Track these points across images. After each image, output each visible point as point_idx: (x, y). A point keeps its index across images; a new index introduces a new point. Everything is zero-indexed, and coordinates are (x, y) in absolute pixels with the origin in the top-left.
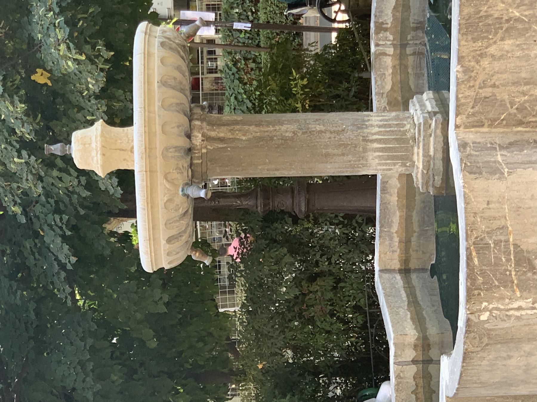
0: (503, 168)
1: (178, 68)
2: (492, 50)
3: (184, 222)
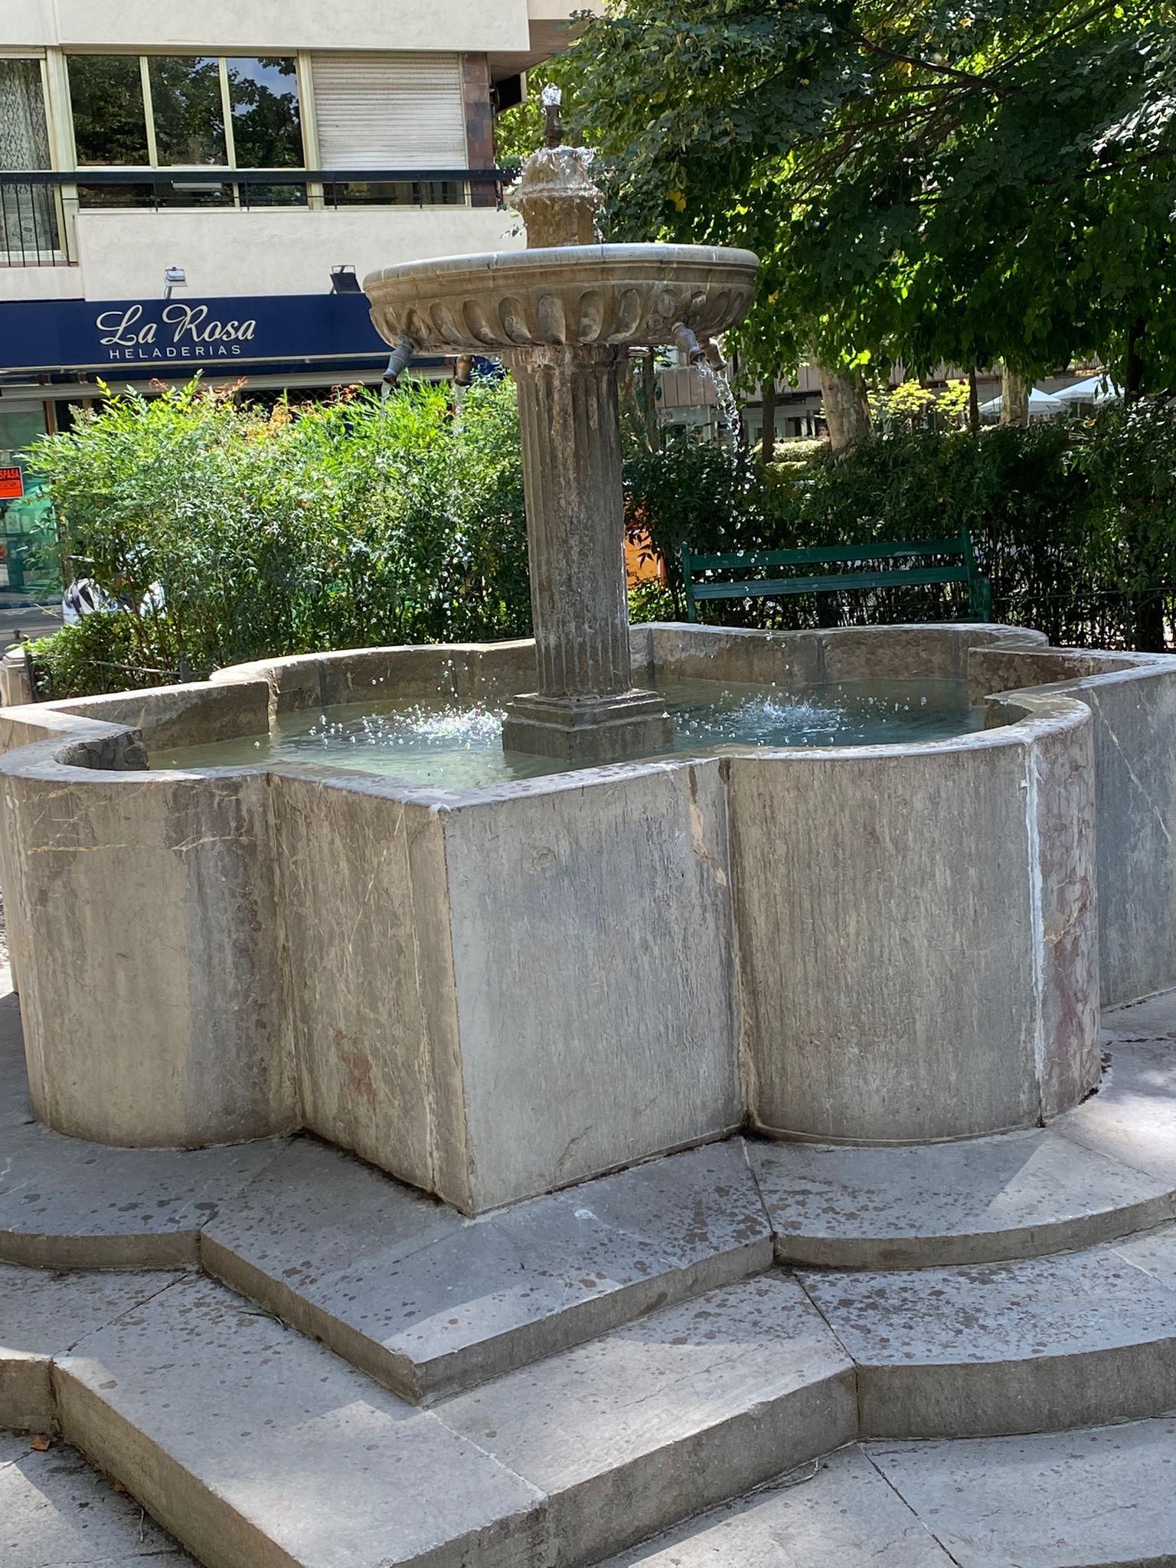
0: (187, 843)
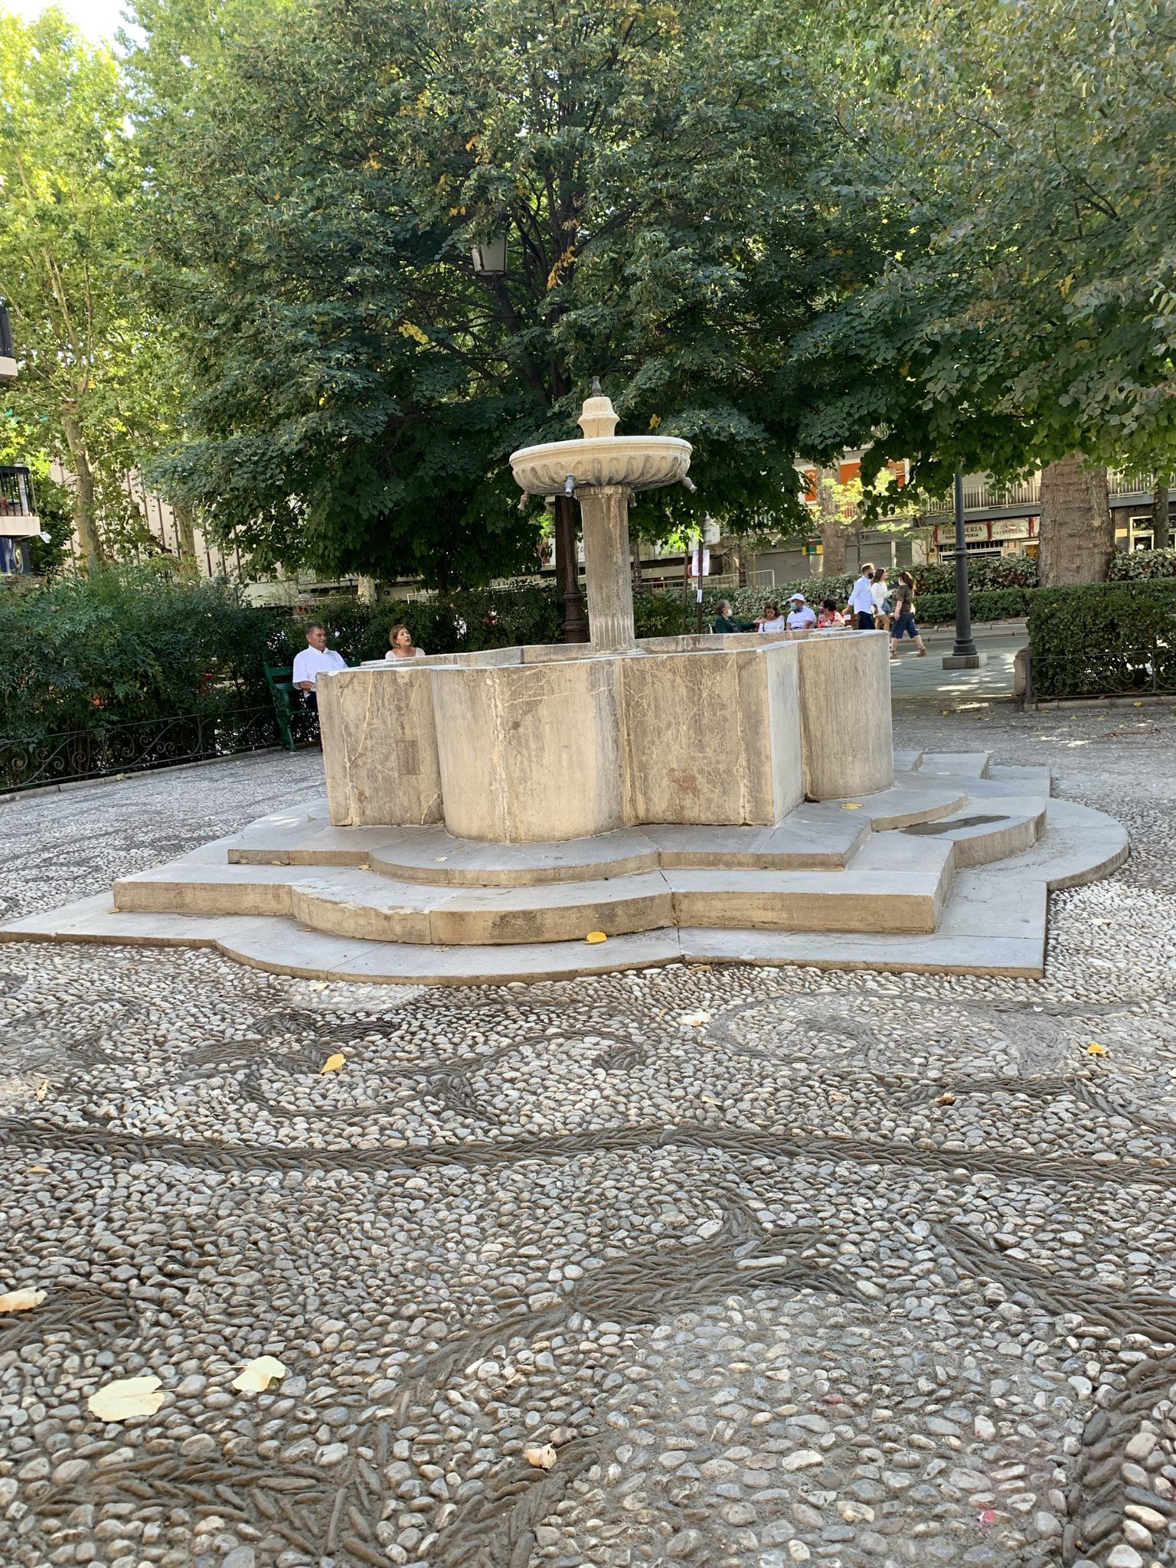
1: (659, 470)
2: (678, 679)
3: (547, 480)
